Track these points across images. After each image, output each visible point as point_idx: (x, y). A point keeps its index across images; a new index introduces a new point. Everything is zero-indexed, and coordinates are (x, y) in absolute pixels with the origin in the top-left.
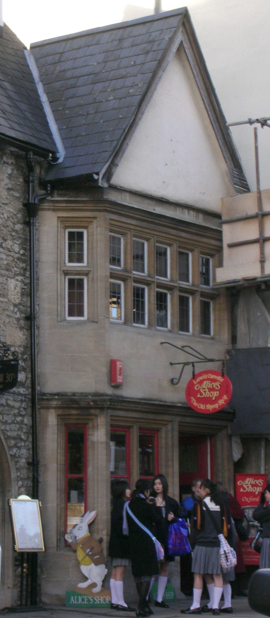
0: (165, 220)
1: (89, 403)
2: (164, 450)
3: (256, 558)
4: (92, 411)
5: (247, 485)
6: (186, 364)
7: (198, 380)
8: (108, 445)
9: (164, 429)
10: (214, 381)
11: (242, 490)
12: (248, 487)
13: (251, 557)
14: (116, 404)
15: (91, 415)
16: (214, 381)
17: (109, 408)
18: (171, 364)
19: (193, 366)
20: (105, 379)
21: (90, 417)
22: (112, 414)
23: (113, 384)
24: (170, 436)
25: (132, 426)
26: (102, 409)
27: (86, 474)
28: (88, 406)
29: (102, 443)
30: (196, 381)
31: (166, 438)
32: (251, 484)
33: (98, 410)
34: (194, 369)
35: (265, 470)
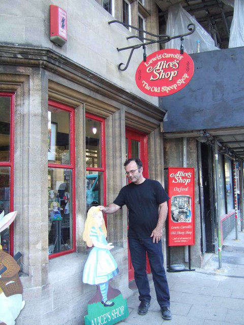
0: (80, 74)
1: (15, 54)
2: (111, 139)
3: (185, 240)
4: (21, 70)
5: (178, 177)
6: (134, 48)
7: (151, 62)
8: (44, 117)
9: (111, 117)
10: (172, 59)
11: (173, 182)
12: (179, 179)
13: (181, 238)
14: (57, 64)
15: (20, 75)
16: (172, 59)
17: (46, 68)
18: (119, 50)
19: (144, 48)
20: (41, 27)
21: (18, 79)
22: (51, 79)
23: (53, 38)
24: (117, 124)
25: (78, 106)
26: (36, 66)
27: (12, 161)
28: (14, 60)
29: (35, 115)
30: (147, 64)
31: (114, 127)
32: (181, 176)
33: (31, 69)
34: (145, 51)
35: (187, 164)
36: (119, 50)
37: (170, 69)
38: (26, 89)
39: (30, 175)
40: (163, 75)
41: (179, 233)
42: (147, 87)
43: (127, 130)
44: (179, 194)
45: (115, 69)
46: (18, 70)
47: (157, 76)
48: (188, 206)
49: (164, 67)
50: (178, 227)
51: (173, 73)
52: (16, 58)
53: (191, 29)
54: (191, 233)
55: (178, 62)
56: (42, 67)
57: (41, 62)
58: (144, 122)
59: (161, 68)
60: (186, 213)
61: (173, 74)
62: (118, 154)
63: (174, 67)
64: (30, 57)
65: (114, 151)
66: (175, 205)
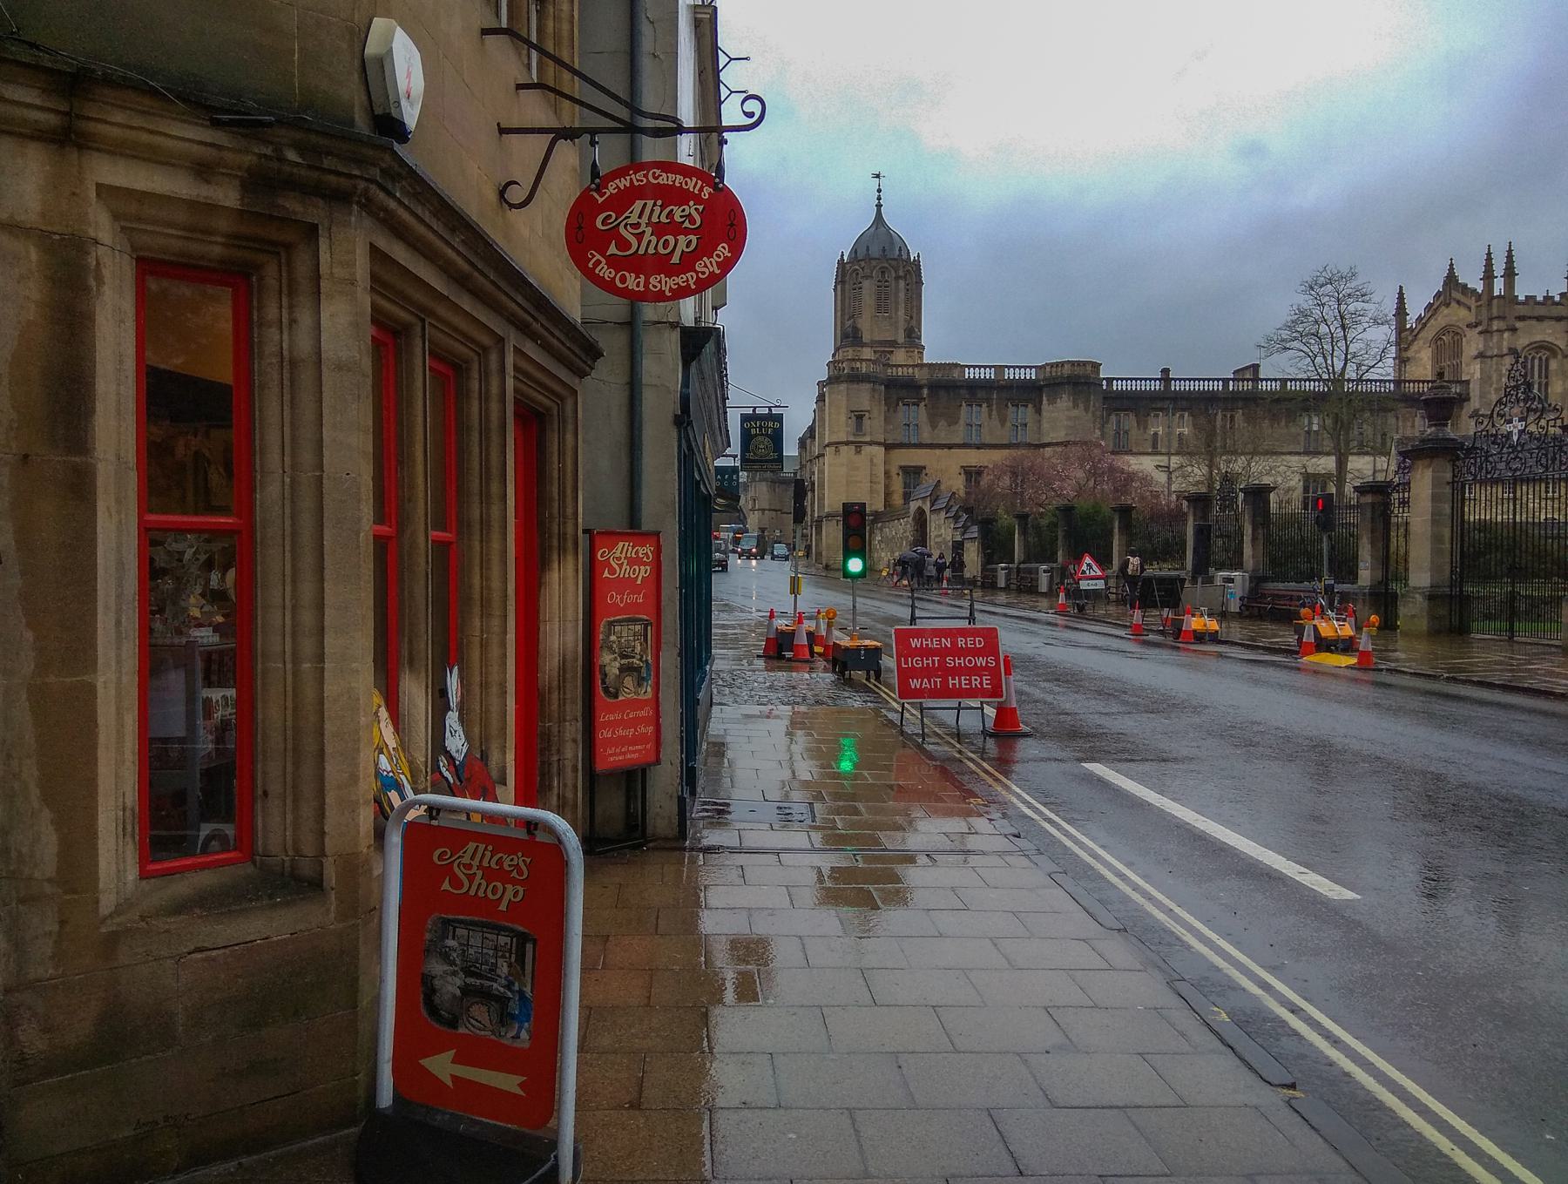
4: (293, 205)
16: (682, 197)
18: (503, 131)
28: (275, 165)
36: (503, 131)
37: (676, 229)
38: (302, 268)
39: (327, 563)
40: (650, 244)
41: (622, 732)
42: (605, 272)
43: (518, 415)
44: (620, 611)
45: (492, 196)
46: (280, 201)
47: (629, 245)
48: (644, 650)
49: (655, 219)
50: (618, 716)
51: (681, 238)
52: (281, 159)
53: (750, 115)
54: (651, 729)
55: (701, 208)
56: (358, 203)
57: (362, 185)
58: (538, 375)
59: (645, 219)
60: (638, 669)
61: (683, 244)
62: (495, 488)
63: (687, 224)
64: (327, 163)
65: (486, 477)
66: (610, 649)
